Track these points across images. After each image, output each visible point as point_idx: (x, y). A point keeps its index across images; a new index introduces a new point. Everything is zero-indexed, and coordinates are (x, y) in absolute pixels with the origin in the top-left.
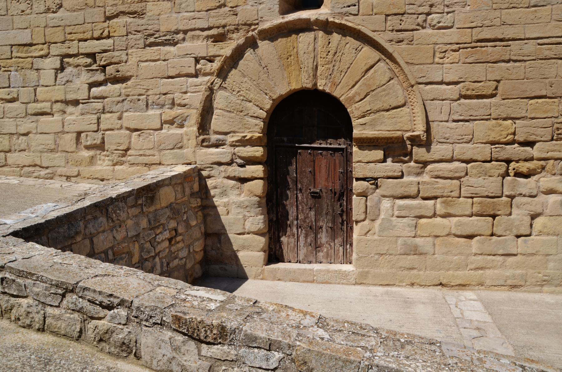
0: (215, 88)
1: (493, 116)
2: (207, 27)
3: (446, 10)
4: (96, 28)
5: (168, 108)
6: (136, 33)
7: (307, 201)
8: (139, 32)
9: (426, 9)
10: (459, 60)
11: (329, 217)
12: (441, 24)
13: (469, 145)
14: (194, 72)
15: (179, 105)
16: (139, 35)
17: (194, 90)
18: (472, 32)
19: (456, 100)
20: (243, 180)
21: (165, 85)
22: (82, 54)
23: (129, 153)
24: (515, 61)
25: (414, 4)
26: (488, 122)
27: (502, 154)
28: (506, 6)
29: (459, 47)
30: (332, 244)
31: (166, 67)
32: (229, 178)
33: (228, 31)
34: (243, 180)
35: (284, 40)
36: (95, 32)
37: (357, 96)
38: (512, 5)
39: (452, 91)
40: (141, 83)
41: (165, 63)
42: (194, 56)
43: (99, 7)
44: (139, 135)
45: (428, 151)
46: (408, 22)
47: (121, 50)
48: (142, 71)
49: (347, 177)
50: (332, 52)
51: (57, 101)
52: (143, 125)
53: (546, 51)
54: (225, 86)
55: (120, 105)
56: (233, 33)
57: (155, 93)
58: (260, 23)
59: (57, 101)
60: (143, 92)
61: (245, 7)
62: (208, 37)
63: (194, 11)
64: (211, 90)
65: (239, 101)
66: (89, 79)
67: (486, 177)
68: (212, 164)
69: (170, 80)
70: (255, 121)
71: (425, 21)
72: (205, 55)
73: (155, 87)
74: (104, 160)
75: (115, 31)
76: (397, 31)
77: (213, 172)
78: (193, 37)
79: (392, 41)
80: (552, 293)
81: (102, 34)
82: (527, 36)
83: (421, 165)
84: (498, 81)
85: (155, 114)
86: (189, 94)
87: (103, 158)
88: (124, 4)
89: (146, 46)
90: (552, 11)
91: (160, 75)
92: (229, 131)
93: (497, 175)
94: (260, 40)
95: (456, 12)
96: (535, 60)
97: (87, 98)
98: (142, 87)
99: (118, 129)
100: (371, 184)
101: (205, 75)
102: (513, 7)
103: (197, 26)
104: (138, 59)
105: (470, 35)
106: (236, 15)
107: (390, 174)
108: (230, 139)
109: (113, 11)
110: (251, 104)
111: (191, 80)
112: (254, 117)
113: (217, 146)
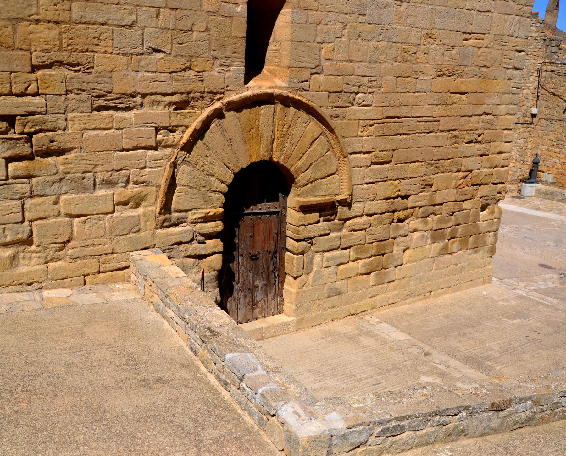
1: (389, 178)
2: (170, 92)
3: (370, 90)
4: (17, 80)
5: (122, 187)
6: (79, 92)
7: (247, 264)
8: (84, 91)
9: (355, 89)
11: (265, 276)
12: (364, 103)
13: (374, 202)
14: (154, 145)
15: (137, 183)
16: (84, 96)
17: (155, 165)
20: (200, 257)
21: (117, 159)
24: (405, 134)
26: (386, 182)
28: (403, 90)
29: (373, 122)
30: (266, 300)
31: (121, 137)
32: (189, 257)
33: (193, 98)
34: (200, 257)
36: (14, 86)
37: (304, 167)
38: (407, 90)
40: (87, 157)
41: (118, 132)
42: (155, 125)
43: (21, 49)
44: (85, 222)
45: (350, 209)
47: (58, 113)
48: (89, 143)
49: (281, 238)
52: (90, 208)
54: (188, 160)
55: (56, 185)
56: (197, 101)
57: (106, 169)
58: (226, 93)
61: (212, 73)
62: (170, 104)
63: (155, 72)
64: (174, 165)
66: (6, 151)
68: (173, 245)
69: (125, 153)
70: (216, 195)
72: (168, 125)
73: (106, 163)
74: (30, 258)
75: (47, 87)
76: (336, 107)
77: (173, 253)
78: (153, 103)
79: (331, 116)
81: (26, 89)
82: (413, 115)
84: (394, 150)
85: (106, 195)
86: (147, 170)
87: (28, 255)
88: (61, 51)
89: (93, 109)
91: (113, 148)
94: (226, 111)
97: (4, 178)
98: (88, 162)
99: (54, 217)
100: (309, 243)
101: (166, 146)
103: (159, 90)
104: (83, 126)
106: (202, 81)
107: (323, 233)
108: (191, 216)
109: (44, 59)
110: (214, 178)
111: (150, 152)
112: (216, 191)
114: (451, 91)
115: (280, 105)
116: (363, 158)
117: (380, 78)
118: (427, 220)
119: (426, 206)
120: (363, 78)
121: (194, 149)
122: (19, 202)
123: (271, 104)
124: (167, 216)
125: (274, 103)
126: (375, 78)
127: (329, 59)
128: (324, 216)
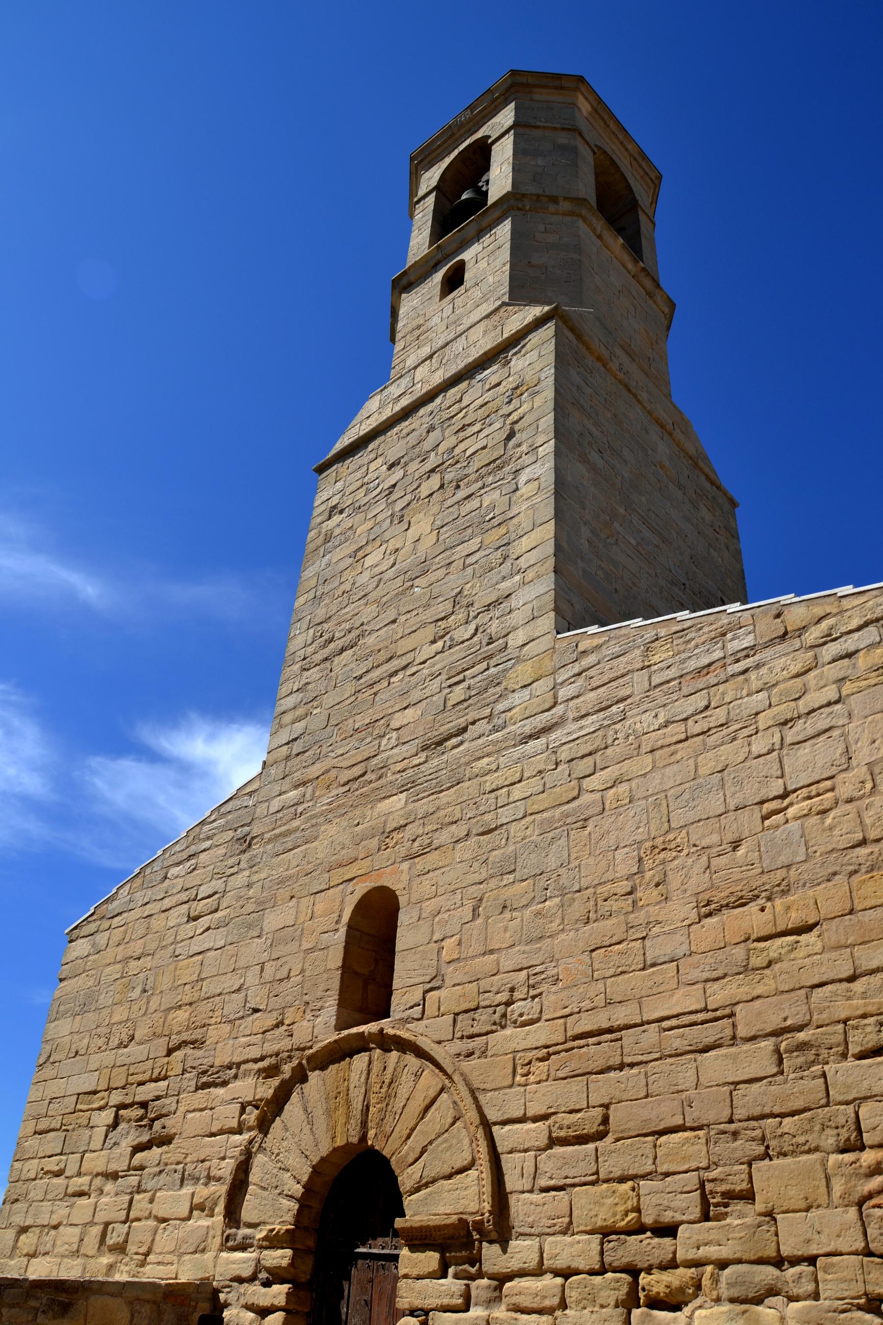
0: (254, 1150)
10: (548, 1075)
14: (236, 1126)
18: (565, 1024)
19: (545, 1150)
22: (137, 1103)
23: (151, 1258)
25: (490, 992)
28: (611, 972)
29: (547, 1052)
35: (337, 1065)
38: (620, 969)
39: (535, 1133)
42: (240, 1100)
45: (505, 1251)
46: (484, 1017)
50: (387, 1081)
51: (97, 1175)
53: (676, 1040)
59: (97, 1175)
60: (181, 1159)
62: (259, 1071)
65: (275, 1171)
67: (596, 1309)
71: (504, 1015)
79: (459, 1054)
83: (495, 1283)
84: (606, 1106)
89: (197, 1088)
90: (678, 971)
91: (201, 1132)
92: (258, 1221)
93: (613, 1303)
95: (544, 994)
96: (660, 1059)
102: (622, 973)
105: (563, 1028)
114: (753, 937)
115: (378, 1051)
116: (528, 1131)
117: (553, 964)
118: (758, 1315)
119: (739, 1261)
120: (517, 973)
121: (271, 1130)
122: (128, 1197)
123: (365, 1051)
124: (233, 1230)
125: (369, 1050)
126: (544, 966)
127: (453, 961)
128: (457, 1264)
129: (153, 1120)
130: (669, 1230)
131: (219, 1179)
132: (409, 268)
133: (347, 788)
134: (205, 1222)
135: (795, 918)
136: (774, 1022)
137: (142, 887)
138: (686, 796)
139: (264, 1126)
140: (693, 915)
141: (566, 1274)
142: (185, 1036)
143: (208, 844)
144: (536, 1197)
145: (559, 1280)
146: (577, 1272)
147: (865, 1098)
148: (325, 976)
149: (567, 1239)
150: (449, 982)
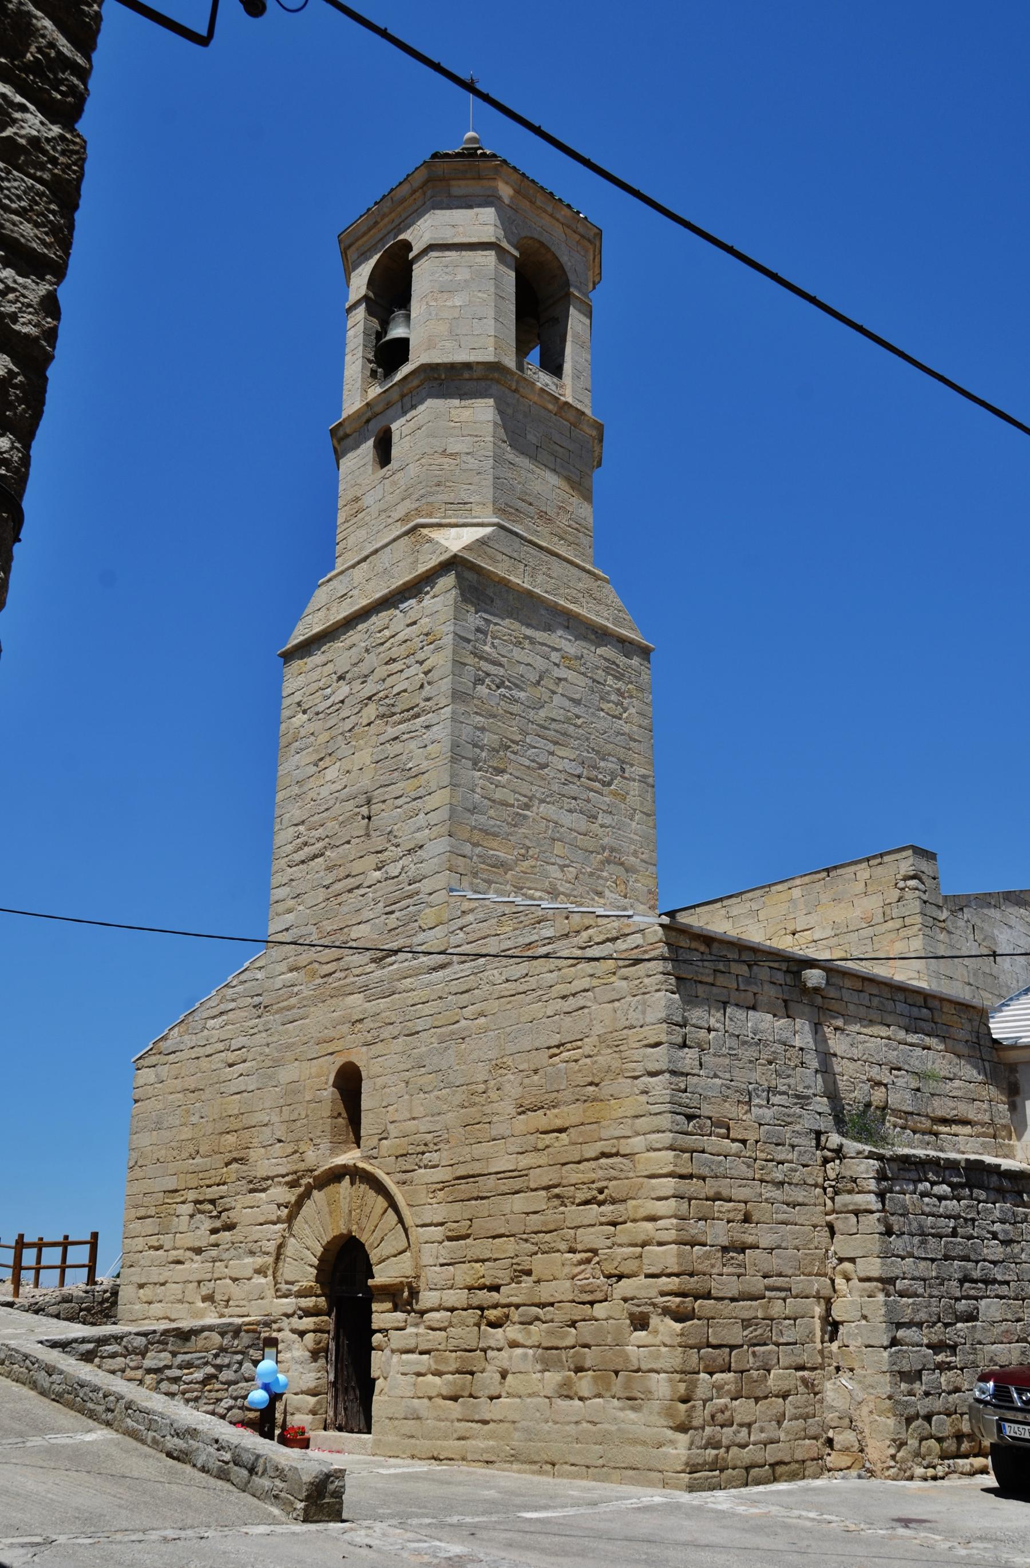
27: (475, 1300)
29: (444, 1185)
39: (438, 1232)
62: (287, 1183)
80: (519, 1471)
84: (471, 1220)
113: (286, 1296)
129: (220, 1213)
130: (496, 1288)
131: (268, 1254)
132: (344, 420)
133: (325, 979)
134: (263, 1280)
135: (558, 1123)
136: (545, 1182)
137: (186, 1032)
138: (513, 1035)
139: (290, 1219)
140: (513, 1112)
141: (452, 1310)
142: (235, 1155)
143: (232, 1005)
144: (438, 1269)
145: (449, 1313)
146: (457, 1309)
147: (580, 1227)
148: (321, 1121)
149: (451, 1291)
150: (392, 1136)
